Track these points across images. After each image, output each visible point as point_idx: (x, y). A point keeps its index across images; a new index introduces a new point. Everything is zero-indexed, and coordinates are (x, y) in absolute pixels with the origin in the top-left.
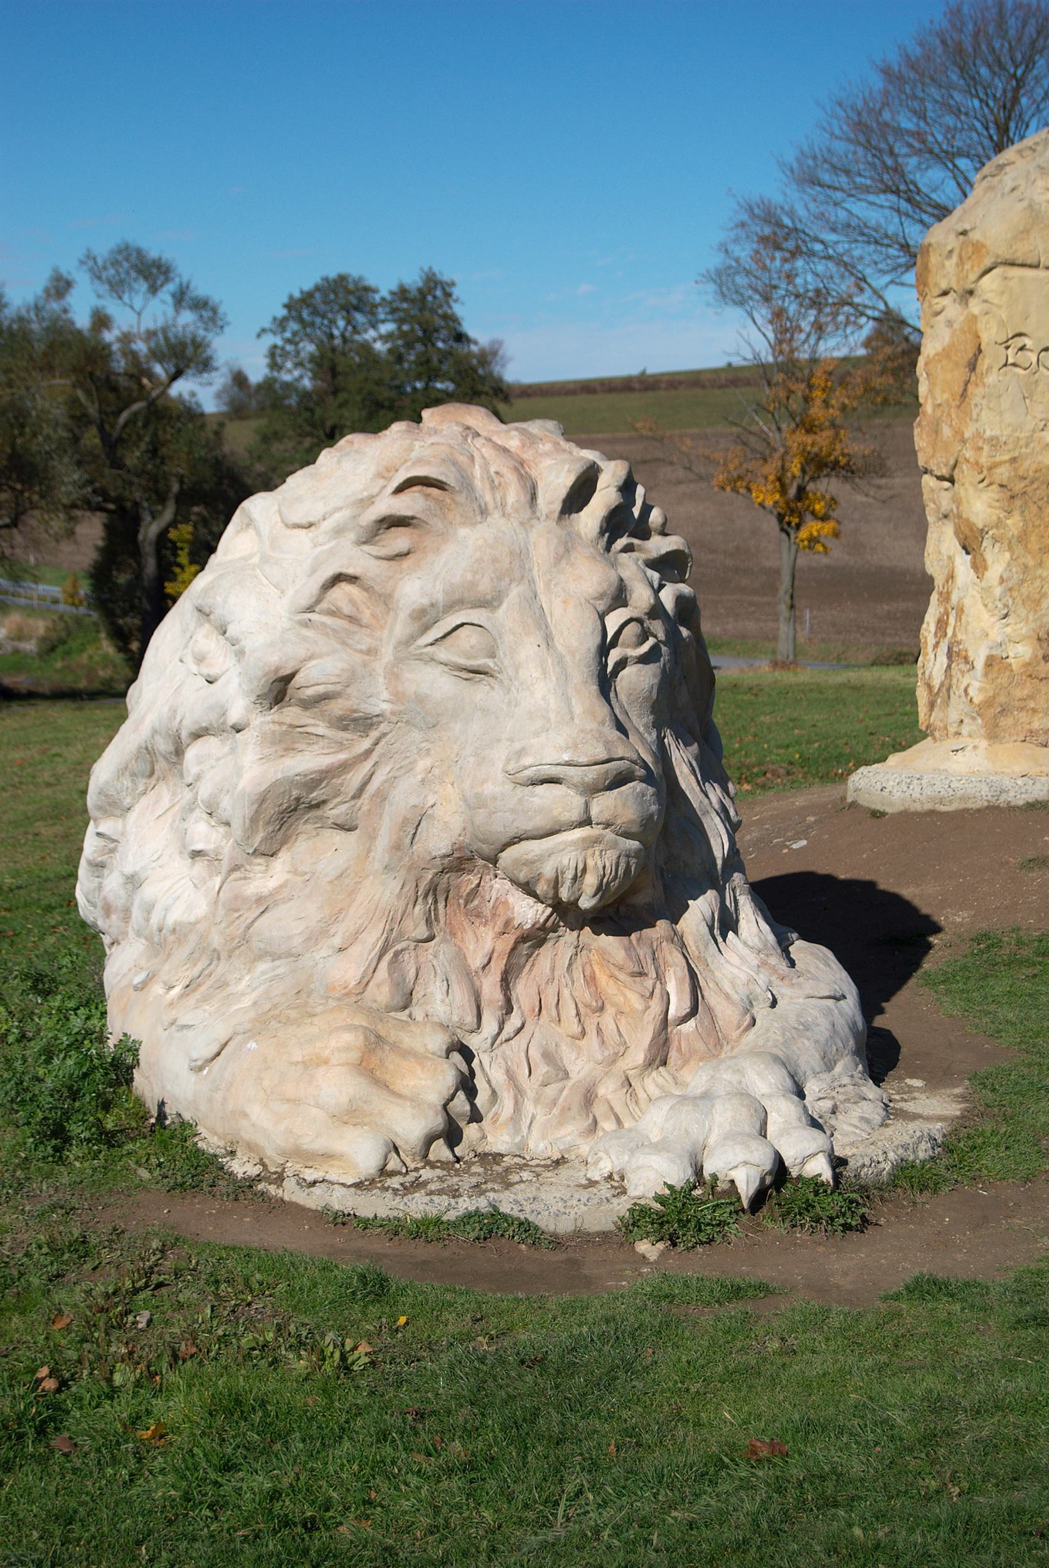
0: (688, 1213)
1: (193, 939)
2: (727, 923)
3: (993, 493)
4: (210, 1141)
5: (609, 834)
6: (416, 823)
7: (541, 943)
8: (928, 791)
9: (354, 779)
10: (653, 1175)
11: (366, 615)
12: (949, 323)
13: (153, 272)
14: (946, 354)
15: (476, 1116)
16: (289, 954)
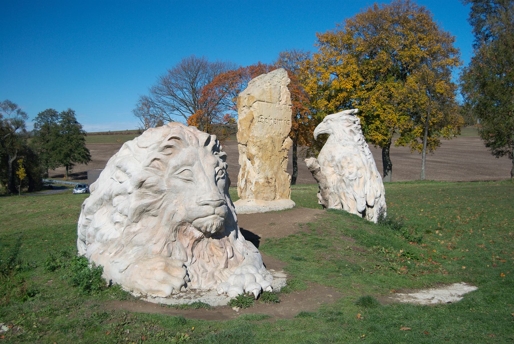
0: (244, 300)
1: (116, 242)
2: (237, 237)
3: (256, 148)
4: (126, 288)
5: (218, 216)
6: (173, 214)
7: (199, 241)
8: (244, 210)
9: (158, 205)
10: (235, 293)
11: (161, 168)
12: (245, 113)
13: (13, 106)
14: (245, 119)
15: (190, 281)
16: (142, 245)
